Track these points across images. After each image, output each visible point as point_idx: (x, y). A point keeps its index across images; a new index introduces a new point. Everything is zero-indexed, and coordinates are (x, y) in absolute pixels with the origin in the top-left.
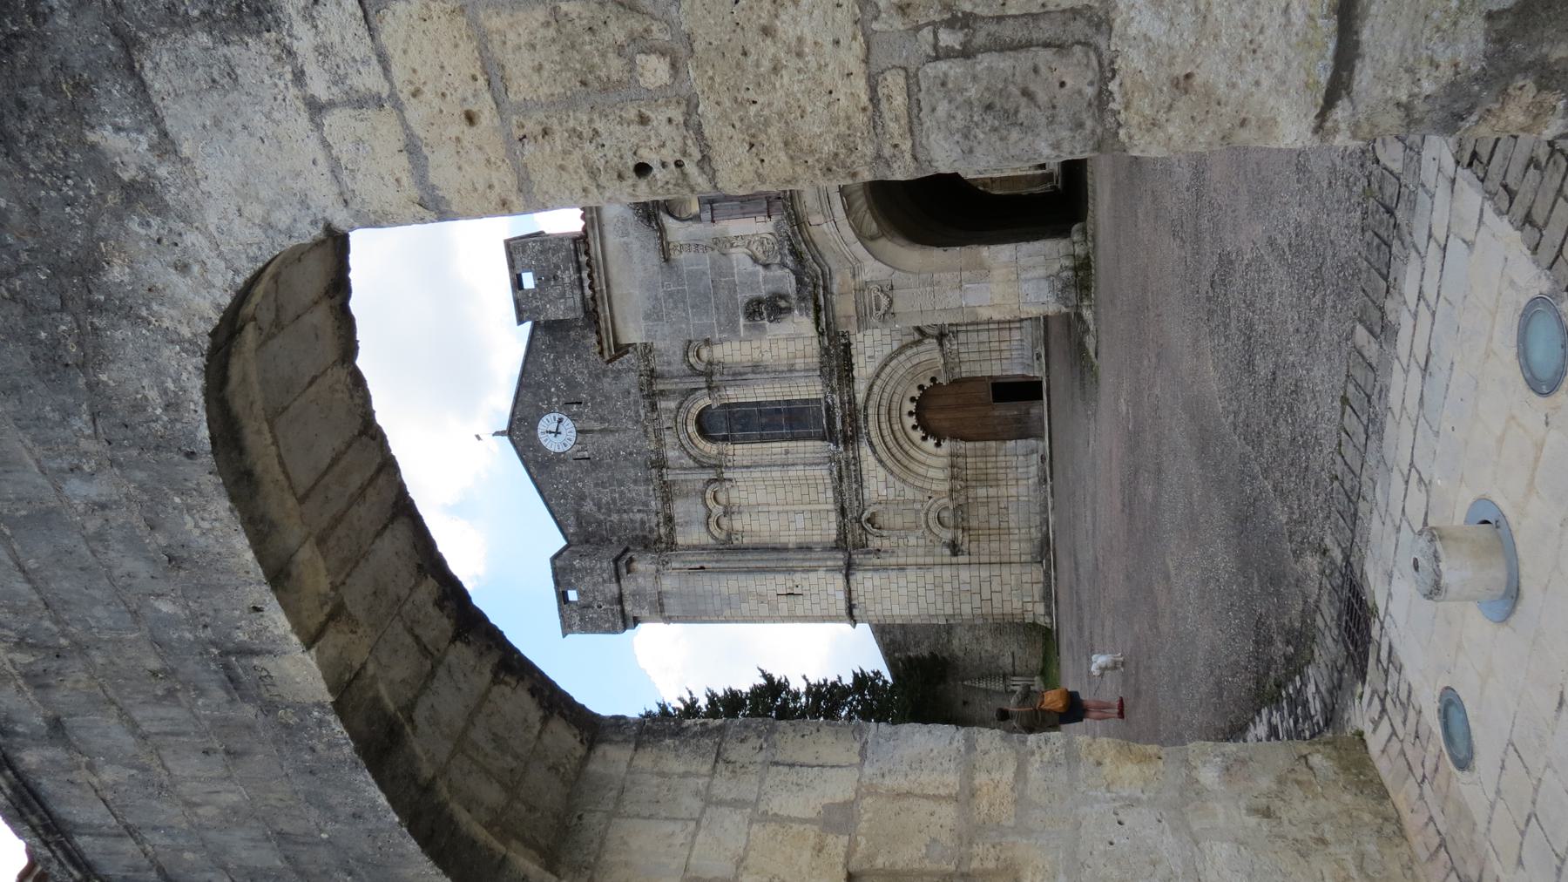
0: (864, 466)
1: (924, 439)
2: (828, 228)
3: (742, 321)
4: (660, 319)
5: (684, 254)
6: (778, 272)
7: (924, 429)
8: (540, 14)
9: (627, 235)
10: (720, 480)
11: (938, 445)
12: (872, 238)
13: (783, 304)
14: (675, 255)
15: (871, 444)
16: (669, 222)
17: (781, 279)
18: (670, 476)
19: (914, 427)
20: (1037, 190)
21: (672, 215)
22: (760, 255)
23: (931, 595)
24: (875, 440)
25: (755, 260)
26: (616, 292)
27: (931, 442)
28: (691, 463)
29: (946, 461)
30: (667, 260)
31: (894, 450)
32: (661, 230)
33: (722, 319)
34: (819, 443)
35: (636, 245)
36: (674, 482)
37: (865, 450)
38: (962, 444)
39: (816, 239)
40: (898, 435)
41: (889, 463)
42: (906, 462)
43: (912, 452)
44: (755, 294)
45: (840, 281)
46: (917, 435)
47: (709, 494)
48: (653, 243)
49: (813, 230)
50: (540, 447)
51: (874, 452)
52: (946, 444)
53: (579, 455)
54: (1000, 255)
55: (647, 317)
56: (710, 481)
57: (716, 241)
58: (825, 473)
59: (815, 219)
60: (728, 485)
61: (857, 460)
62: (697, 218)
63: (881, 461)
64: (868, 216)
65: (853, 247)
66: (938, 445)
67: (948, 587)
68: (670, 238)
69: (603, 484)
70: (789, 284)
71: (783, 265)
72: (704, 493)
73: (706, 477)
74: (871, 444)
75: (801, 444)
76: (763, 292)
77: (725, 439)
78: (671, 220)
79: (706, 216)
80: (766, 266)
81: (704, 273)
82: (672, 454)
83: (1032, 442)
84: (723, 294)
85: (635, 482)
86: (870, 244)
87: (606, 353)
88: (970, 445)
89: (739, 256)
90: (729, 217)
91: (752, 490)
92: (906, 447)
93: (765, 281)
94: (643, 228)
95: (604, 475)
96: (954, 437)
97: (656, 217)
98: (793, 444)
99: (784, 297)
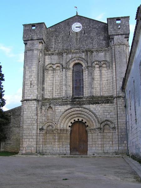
23: (29, 122)
37: (69, 106)
50: (73, 22)
51: (69, 109)
61: (67, 104)
63: (66, 110)
67: (31, 127)
88: (69, 135)
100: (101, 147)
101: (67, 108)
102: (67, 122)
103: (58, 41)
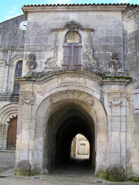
0: (5, 102)
1: (10, 119)
2: (56, 85)
3: (29, 53)
4: (34, 27)
5: (54, 36)
6: (44, 66)
7: (13, 119)
8: (138, 5)
9: (63, 20)
10: (6, 65)
11: (8, 122)
12: (51, 100)
13: (32, 67)
14: (54, 33)
15: (9, 104)
16: (65, 32)
17: (41, 67)
18: (9, 52)
19: (13, 116)
20: (72, 153)
21: (67, 33)
22: (50, 61)
24: (11, 106)
25: (49, 59)
26: (45, 14)
27: (9, 120)
28: (12, 58)
29: (3, 124)
30: (53, 30)
31: (8, 110)
32: (63, 30)
33: (31, 47)
34: (12, 91)
35: (59, 22)
36: (7, 53)
37: (8, 102)
38: (7, 128)
39: (53, 81)
40: (12, 112)
41: (4, 109)
42: (4, 113)
43: (7, 115)
44: (37, 58)
45: (38, 87)
46: (11, 117)
47: (3, 62)
48: (59, 27)
49: (56, 80)
50: (21, 21)
51: (7, 105)
52: (8, 124)
53: (18, 31)
54: (40, 143)
55: (35, 23)
56: (6, 62)
57: (57, 47)
58: (4, 92)
59: (60, 80)
60: (5, 66)
61: (6, 100)
62: (65, 41)
63: (5, 106)
64: (59, 100)
65: (48, 93)
66: (8, 122)
68: (60, 32)
69: (10, 35)
70: (38, 70)
71: (46, 68)
72: (3, 60)
73: (8, 61)
74: (9, 104)
75: (13, 86)
76: (38, 61)
77: (17, 67)
78: (66, 33)
79: (66, 45)
80: (46, 63)
81: (47, 42)
82: (15, 53)
83: (5, 147)
84: (39, 48)
85: (9, 43)
86: (49, 99)
87: (25, 8)
88: (7, 130)
89: (50, 54)
90: (64, 53)
91: (3, 72)
92: (8, 114)
93: (41, 62)
94: (65, 24)
95: (12, 35)
96: (9, 126)
97: (67, 28)
98: (13, 84)
99: (35, 67)
100: (112, 116)
101: (6, 104)
102: (5, 117)
103: (5, 38)
